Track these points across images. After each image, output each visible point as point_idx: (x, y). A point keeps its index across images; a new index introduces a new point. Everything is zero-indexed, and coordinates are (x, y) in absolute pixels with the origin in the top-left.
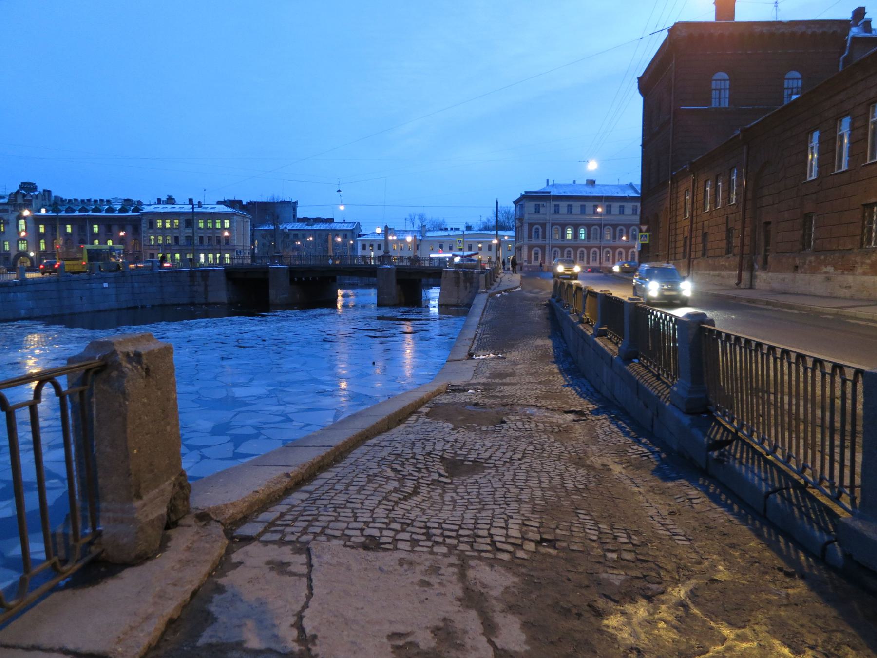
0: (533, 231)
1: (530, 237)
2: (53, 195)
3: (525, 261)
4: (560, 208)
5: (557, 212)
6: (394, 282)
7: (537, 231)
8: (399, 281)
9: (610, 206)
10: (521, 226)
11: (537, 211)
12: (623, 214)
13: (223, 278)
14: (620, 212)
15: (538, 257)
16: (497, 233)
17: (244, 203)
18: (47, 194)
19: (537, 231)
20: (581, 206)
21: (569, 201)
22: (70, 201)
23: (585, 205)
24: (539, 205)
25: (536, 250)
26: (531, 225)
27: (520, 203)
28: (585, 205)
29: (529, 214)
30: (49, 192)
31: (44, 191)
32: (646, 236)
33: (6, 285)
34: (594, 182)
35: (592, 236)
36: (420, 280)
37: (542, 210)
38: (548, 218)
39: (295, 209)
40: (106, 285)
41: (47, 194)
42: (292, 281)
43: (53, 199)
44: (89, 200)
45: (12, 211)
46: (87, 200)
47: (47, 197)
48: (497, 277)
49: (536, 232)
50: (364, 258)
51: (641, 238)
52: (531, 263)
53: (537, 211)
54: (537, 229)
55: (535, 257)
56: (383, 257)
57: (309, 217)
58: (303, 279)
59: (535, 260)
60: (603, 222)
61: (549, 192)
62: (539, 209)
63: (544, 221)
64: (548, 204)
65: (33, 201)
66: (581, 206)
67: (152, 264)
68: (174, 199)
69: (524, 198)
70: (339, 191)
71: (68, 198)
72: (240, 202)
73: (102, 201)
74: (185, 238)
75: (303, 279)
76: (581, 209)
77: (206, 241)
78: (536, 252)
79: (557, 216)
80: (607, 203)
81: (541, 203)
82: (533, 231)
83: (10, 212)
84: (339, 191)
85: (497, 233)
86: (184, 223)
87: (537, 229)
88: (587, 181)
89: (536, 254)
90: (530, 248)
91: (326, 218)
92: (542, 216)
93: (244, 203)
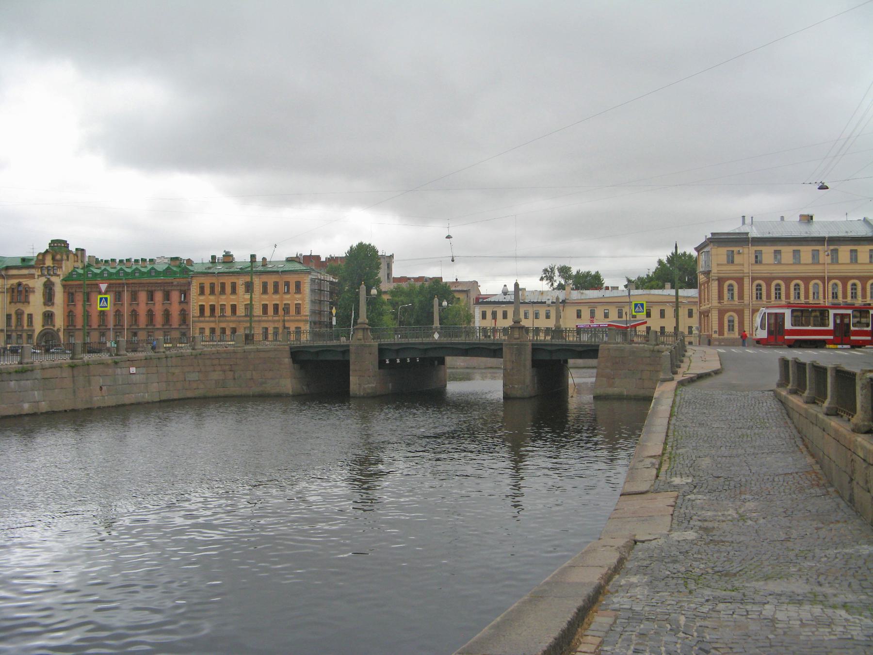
0: (849, 287)
1: (720, 297)
2: (87, 254)
3: (715, 332)
4: (859, 254)
5: (758, 260)
6: (529, 363)
7: (731, 288)
8: (536, 363)
9: (836, 251)
10: (708, 282)
11: (731, 261)
12: (856, 262)
13: (287, 360)
14: (851, 259)
15: (733, 326)
16: (677, 293)
17: (323, 259)
18: (79, 253)
19: (731, 288)
20: (851, 251)
21: (777, 245)
22: (106, 261)
23: (856, 251)
24: (733, 251)
25: (731, 316)
26: (721, 281)
27: (705, 250)
28: (856, 251)
29: (718, 265)
30: (83, 250)
31: (77, 249)
32: (106, 299)
33: (870, 371)
34: (812, 217)
35: (815, 297)
36: (566, 362)
37: (737, 259)
38: (746, 271)
39: (389, 267)
40: (133, 370)
41: (79, 253)
42: (381, 364)
43: (87, 259)
44: (128, 260)
45: (38, 276)
46: (126, 260)
47: (79, 257)
48: (684, 356)
49: (729, 290)
50: (484, 330)
51: (101, 301)
52: (723, 334)
53: (731, 261)
54: (731, 285)
55: (729, 326)
56: (512, 327)
57: (408, 276)
58: (398, 361)
59: (729, 330)
60: (826, 275)
61: (747, 234)
62: (733, 257)
63: (742, 275)
64: (746, 250)
65: (64, 262)
66: (851, 251)
67: (17, 341)
68: (232, 256)
69: (711, 242)
70: (448, 237)
71: (105, 259)
72: (318, 257)
73: (144, 260)
74: (244, 307)
75: (398, 361)
76: (794, 256)
77: (271, 310)
78: (731, 318)
79: (757, 268)
80: (832, 247)
81: (736, 249)
82: (849, 287)
83: (36, 277)
84: (448, 237)
85: (677, 293)
86: (244, 286)
87: (797, 285)
88: (801, 216)
89: (731, 322)
90: (722, 313)
91: (431, 277)
92: (738, 268)
93: (323, 259)
